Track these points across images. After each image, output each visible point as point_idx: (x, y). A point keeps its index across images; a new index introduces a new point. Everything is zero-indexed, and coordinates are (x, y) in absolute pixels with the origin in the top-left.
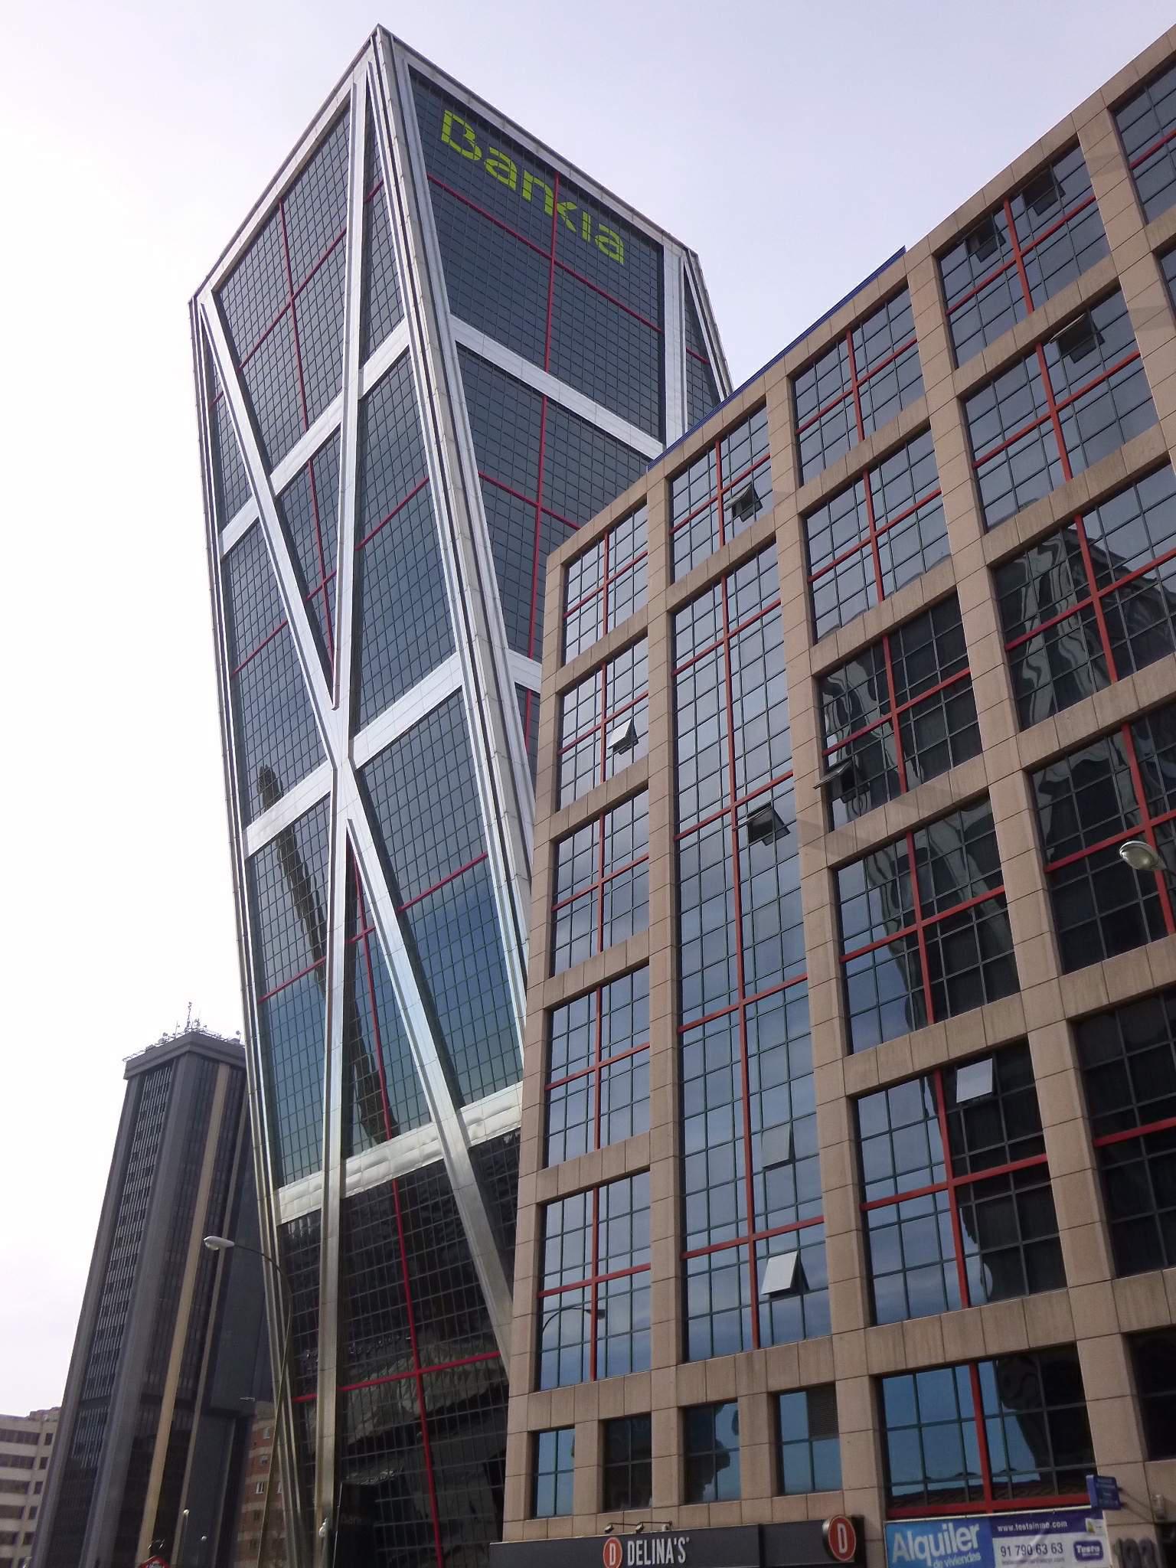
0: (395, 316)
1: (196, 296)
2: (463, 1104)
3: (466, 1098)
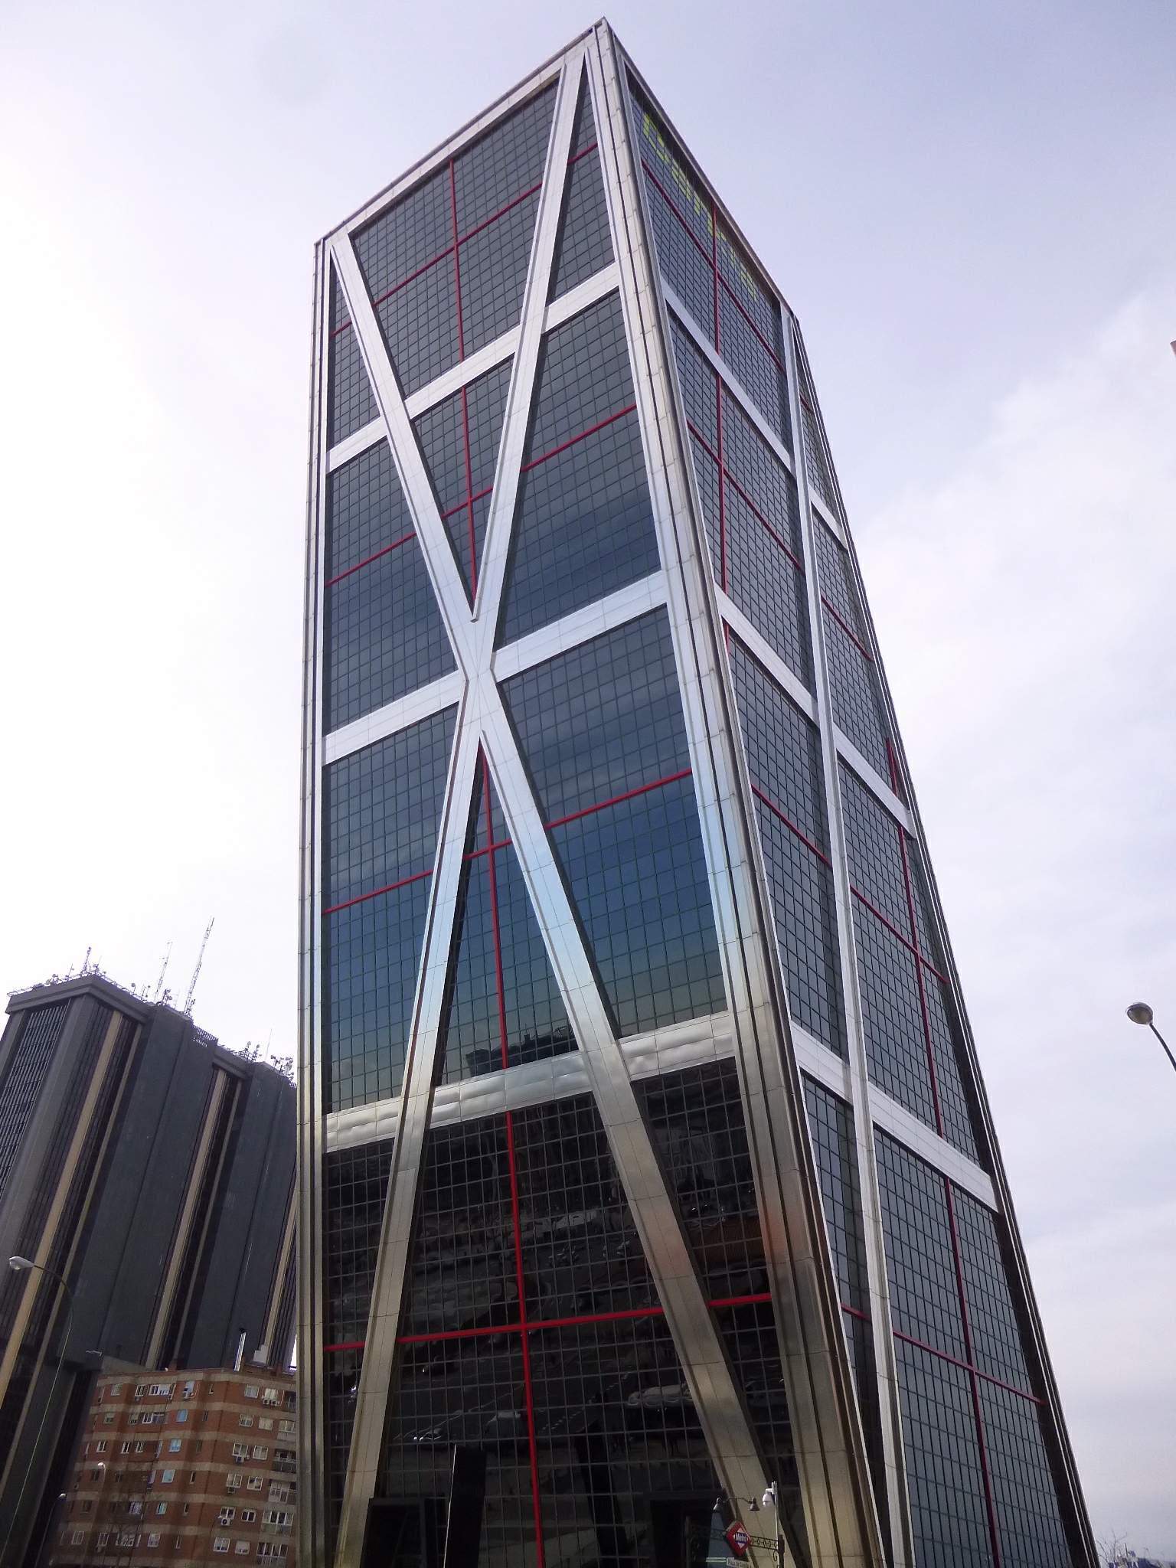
0: (512, 319)
1: (325, 239)
2: (439, 1084)
3: (335, 1106)
